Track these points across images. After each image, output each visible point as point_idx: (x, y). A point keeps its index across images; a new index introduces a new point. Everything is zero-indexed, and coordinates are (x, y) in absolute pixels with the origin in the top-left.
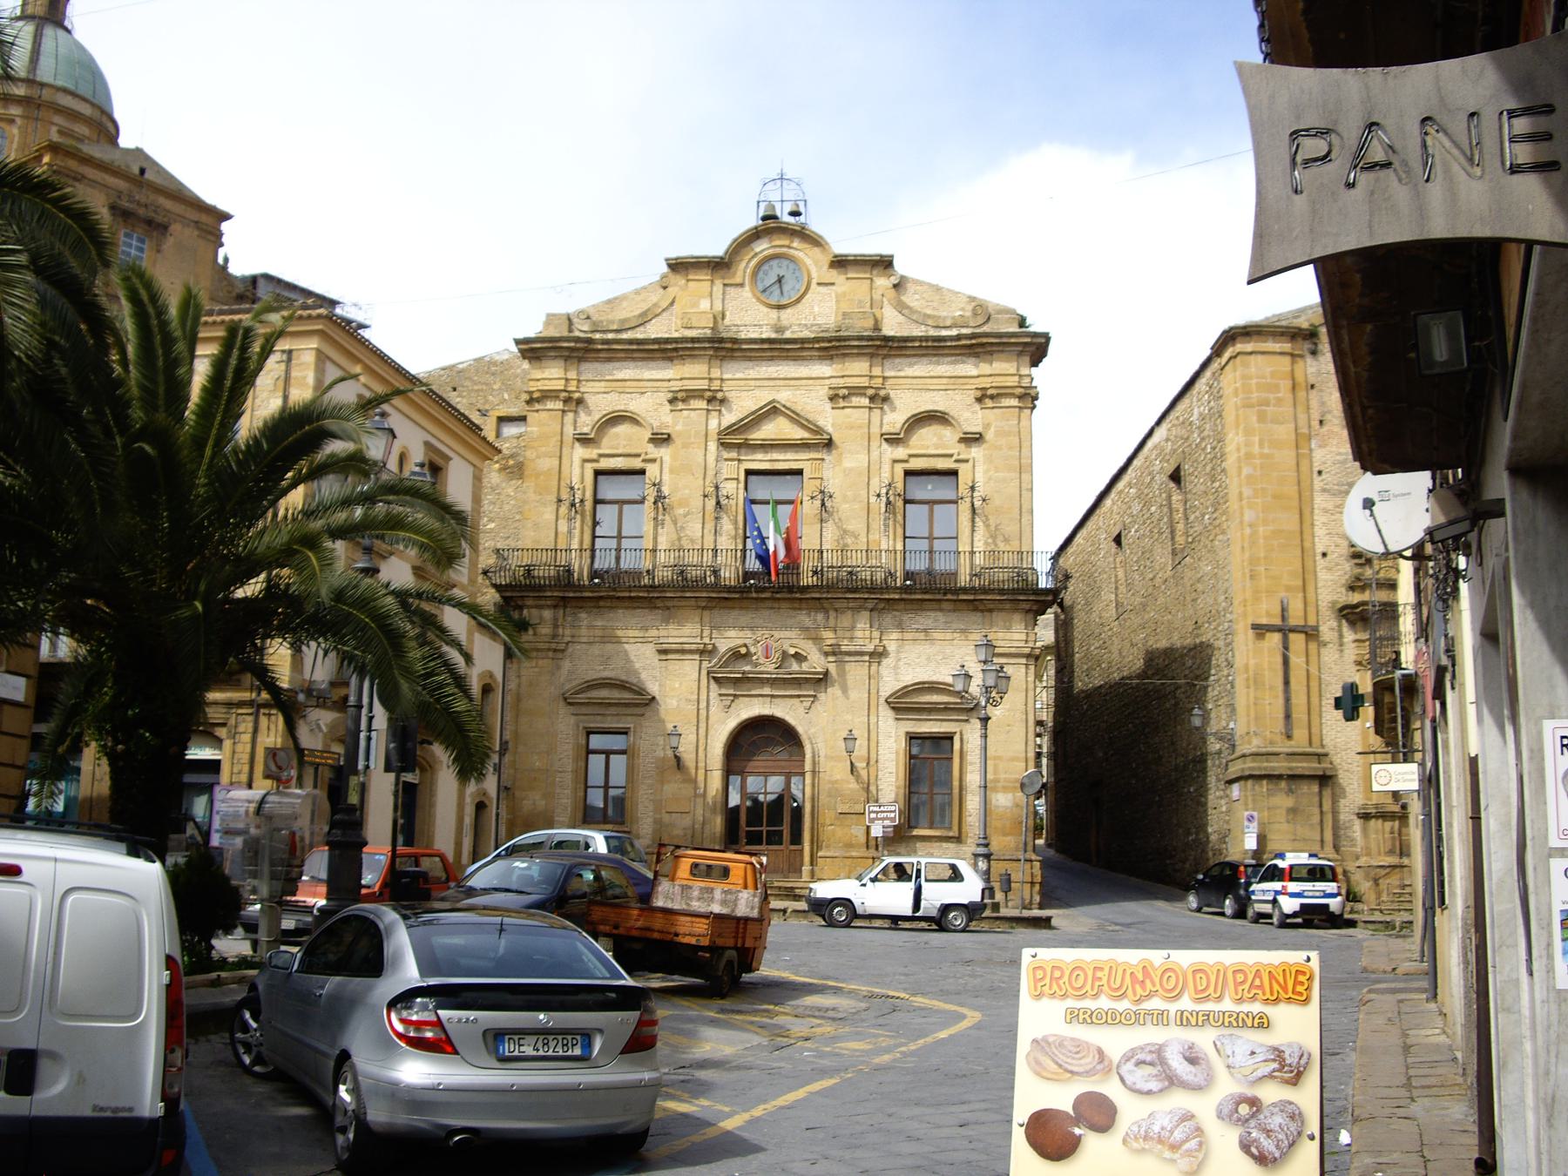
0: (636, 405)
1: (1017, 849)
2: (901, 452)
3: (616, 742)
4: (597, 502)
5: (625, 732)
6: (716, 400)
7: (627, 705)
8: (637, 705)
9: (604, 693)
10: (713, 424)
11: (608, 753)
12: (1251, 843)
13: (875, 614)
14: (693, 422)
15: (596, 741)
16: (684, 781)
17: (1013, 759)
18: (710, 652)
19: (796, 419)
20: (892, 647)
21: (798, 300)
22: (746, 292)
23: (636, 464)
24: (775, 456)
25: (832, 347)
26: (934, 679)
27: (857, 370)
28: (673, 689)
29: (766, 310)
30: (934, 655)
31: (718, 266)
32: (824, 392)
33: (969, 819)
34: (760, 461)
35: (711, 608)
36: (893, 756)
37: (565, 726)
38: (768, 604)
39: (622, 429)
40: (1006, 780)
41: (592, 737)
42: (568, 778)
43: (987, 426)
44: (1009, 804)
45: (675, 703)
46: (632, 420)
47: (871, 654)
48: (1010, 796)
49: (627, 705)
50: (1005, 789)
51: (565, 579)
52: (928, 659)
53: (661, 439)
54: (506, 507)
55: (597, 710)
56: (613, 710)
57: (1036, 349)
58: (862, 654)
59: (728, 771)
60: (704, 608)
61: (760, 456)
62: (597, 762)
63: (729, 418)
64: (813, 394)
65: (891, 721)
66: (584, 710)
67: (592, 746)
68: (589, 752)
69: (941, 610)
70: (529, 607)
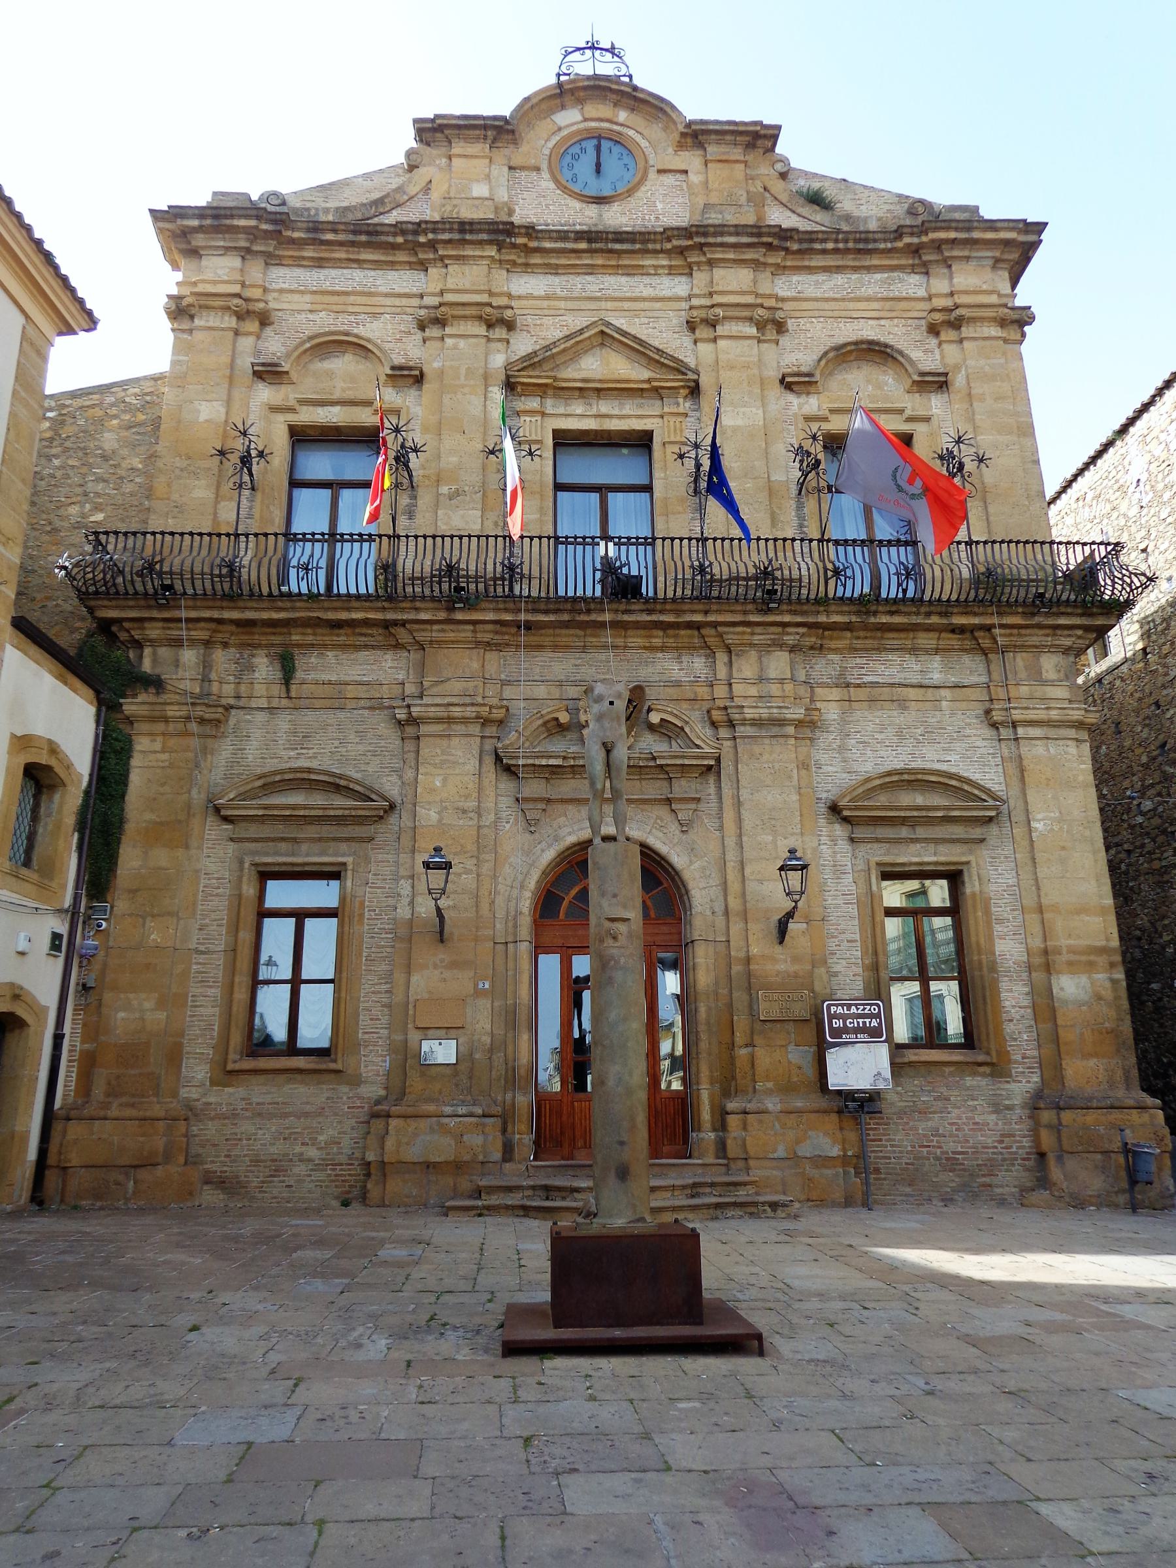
0: (372, 330)
1: (1112, 1084)
2: (812, 404)
3: (323, 894)
4: (295, 484)
5: (333, 874)
6: (498, 321)
7: (340, 820)
8: (360, 820)
9: (296, 798)
10: (498, 360)
11: (300, 916)
12: (1092, 1062)
13: (799, 658)
14: (465, 353)
15: (280, 894)
16: (454, 965)
17: (1081, 910)
18: (501, 722)
19: (639, 349)
20: (831, 713)
21: (630, 192)
22: (546, 183)
23: (366, 417)
24: (604, 407)
25: (689, 245)
26: (918, 764)
27: (734, 281)
28: (432, 790)
29: (577, 205)
30: (913, 719)
31: (496, 132)
32: (676, 319)
33: (1009, 1028)
34: (579, 417)
35: (498, 647)
36: (853, 910)
37: (214, 860)
38: (608, 637)
39: (343, 364)
40: (1072, 950)
41: (271, 884)
42: (216, 966)
43: (957, 368)
44: (1083, 996)
45: (434, 816)
46: (361, 348)
47: (799, 724)
48: (1084, 980)
49: (340, 820)
50: (1073, 967)
51: (229, 586)
52: (900, 734)
53: (410, 376)
54: (128, 488)
55: (280, 830)
56: (312, 831)
57: (1018, 245)
58: (781, 722)
59: (647, 852)
60: (488, 645)
61: (578, 408)
62: (277, 937)
63: (523, 345)
64: (662, 324)
65: (844, 846)
66: (253, 831)
67: (271, 902)
68: (266, 914)
69: (914, 651)
70: (153, 642)
